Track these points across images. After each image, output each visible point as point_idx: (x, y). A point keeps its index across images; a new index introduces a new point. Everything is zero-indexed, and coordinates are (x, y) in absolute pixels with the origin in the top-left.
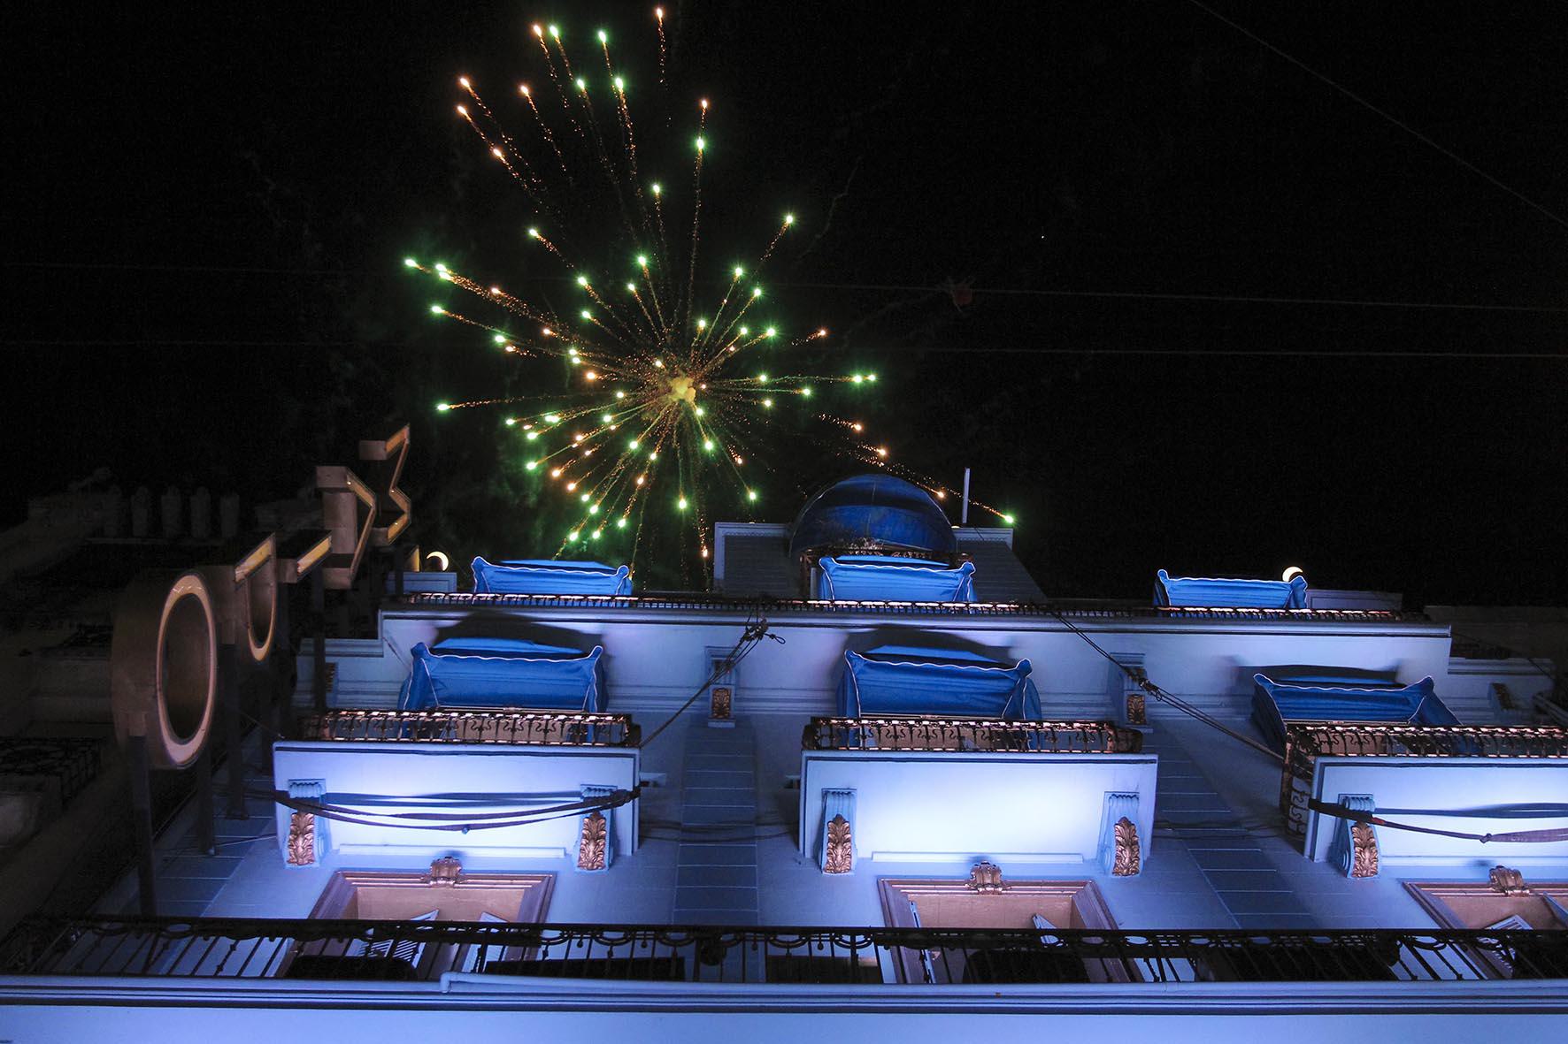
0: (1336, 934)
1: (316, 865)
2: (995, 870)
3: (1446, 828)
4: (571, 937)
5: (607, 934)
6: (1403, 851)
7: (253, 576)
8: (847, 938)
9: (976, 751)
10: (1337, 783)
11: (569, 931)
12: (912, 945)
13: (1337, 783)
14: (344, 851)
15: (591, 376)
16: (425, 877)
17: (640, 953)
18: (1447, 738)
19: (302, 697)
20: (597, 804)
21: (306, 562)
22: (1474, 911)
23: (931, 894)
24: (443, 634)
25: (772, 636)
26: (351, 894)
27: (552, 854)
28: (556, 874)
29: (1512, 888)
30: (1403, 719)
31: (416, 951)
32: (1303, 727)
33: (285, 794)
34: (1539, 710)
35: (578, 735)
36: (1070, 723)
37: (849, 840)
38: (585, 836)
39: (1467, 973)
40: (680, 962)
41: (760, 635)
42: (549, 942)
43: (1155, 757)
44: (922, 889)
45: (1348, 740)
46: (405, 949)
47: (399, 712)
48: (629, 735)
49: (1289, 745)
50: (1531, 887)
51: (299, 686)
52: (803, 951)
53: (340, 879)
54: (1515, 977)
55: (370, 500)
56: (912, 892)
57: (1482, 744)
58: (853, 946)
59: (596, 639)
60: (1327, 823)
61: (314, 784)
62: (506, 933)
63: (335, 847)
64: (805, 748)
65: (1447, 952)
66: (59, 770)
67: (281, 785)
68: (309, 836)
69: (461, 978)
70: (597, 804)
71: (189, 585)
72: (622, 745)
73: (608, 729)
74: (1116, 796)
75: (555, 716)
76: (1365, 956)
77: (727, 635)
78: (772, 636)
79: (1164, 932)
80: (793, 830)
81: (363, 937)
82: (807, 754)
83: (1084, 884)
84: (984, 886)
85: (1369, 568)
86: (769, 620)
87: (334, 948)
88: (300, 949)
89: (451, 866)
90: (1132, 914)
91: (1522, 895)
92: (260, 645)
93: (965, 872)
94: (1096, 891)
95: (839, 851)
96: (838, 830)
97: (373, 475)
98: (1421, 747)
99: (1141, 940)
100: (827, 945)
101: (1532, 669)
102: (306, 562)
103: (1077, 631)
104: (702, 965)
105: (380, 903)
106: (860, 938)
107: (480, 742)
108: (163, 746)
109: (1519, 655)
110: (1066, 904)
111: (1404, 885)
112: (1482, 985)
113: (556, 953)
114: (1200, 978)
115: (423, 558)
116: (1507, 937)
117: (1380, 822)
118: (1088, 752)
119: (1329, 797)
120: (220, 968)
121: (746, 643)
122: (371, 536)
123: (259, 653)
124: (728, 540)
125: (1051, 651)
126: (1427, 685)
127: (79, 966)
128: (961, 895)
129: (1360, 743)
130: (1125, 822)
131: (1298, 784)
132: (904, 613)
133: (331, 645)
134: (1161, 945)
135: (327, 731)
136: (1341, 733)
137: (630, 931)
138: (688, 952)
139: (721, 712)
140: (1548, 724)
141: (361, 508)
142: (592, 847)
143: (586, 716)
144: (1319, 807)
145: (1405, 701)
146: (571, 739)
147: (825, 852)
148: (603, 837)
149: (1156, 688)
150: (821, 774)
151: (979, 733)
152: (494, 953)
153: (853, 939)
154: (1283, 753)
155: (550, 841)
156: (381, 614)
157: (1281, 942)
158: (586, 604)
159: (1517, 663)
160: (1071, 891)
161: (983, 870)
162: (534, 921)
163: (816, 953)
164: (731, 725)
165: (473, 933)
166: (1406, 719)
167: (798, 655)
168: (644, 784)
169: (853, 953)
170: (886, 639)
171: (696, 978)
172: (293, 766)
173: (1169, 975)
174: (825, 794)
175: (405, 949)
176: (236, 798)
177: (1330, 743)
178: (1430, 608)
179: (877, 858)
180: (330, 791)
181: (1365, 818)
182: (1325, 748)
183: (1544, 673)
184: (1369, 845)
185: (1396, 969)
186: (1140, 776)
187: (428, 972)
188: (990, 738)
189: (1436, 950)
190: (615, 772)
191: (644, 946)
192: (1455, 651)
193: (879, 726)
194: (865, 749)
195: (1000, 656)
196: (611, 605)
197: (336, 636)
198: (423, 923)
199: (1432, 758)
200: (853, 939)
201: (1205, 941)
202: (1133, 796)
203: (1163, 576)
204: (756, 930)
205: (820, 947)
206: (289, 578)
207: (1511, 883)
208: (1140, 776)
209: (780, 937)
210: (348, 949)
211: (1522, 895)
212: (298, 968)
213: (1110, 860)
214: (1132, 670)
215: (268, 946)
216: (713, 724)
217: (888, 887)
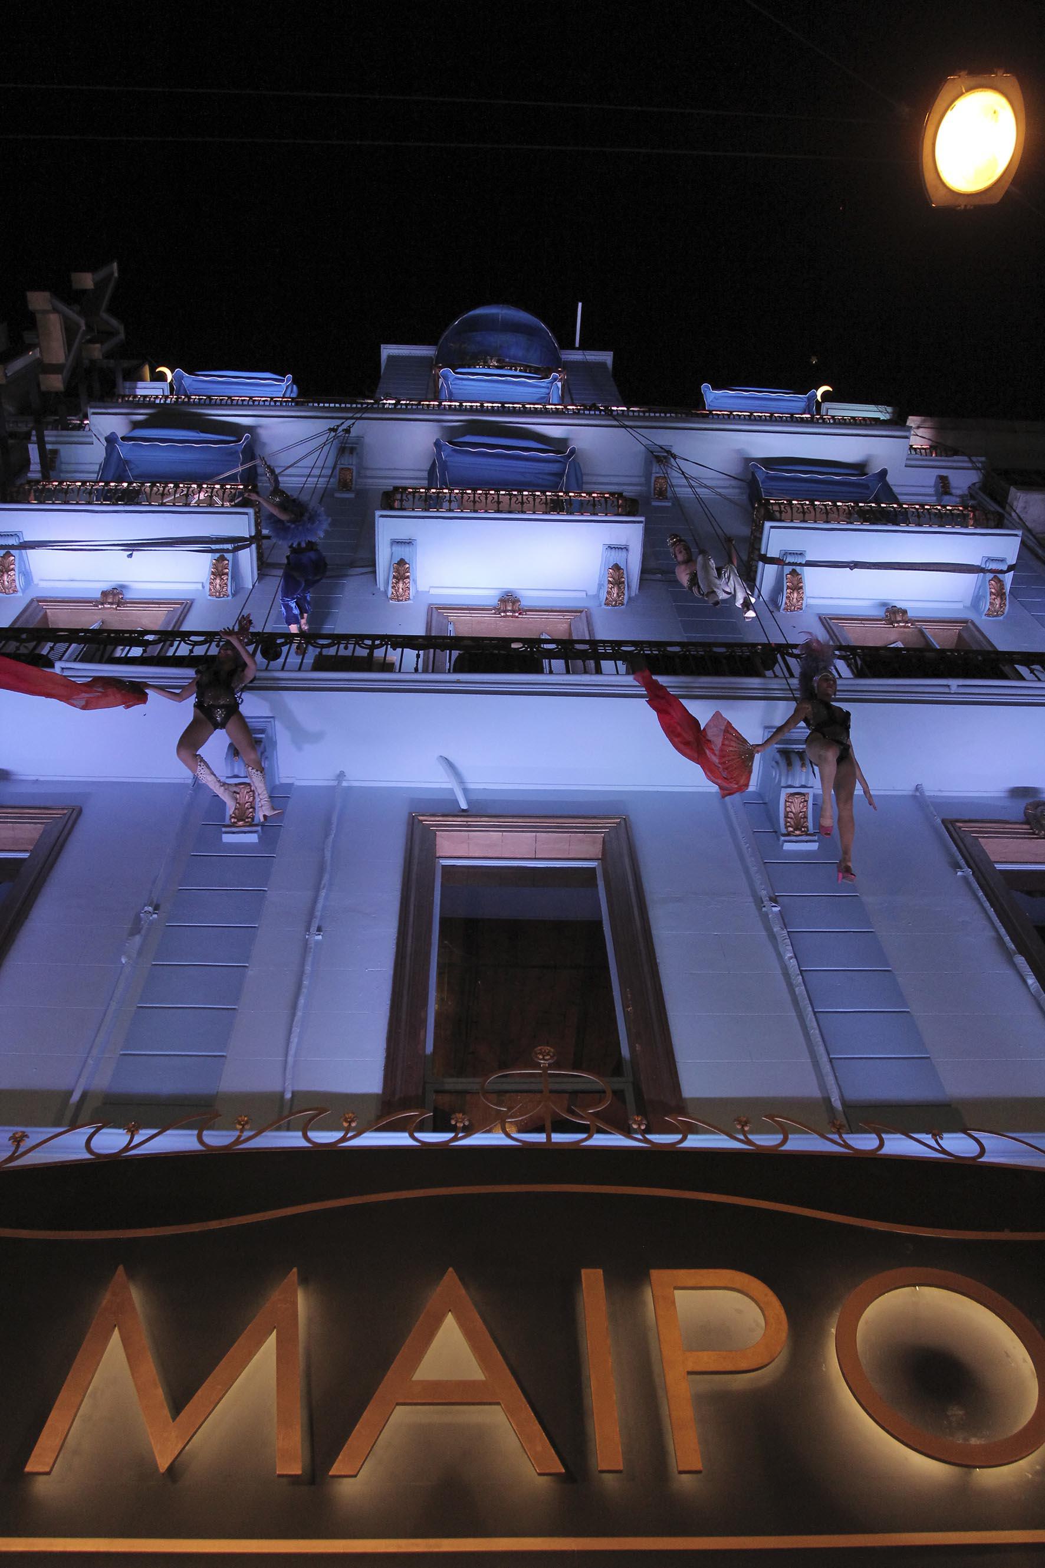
1: (20, 594)
5: (193, 638)
8: (369, 642)
9: (510, 512)
14: (43, 584)
16: (96, 603)
23: (466, 617)
24: (136, 425)
26: (41, 614)
29: (898, 622)
37: (408, 577)
38: (213, 573)
44: (459, 613)
50: (913, 622)
51: (32, 467)
53: (35, 604)
56: (453, 616)
57: (896, 515)
59: (250, 429)
63: (36, 581)
68: (11, 573)
70: (220, 548)
83: (581, 612)
84: (505, 612)
89: (114, 595)
91: (904, 627)
93: (495, 602)
95: (401, 585)
96: (401, 571)
100: (351, 647)
101: (970, 465)
103: (625, 427)
106: (377, 642)
109: (963, 454)
110: (565, 626)
111: (820, 618)
119: (772, 553)
124: (391, 358)
125: (601, 443)
126: (884, 473)
128: (488, 617)
130: (616, 567)
132: (492, 412)
134: (616, 650)
139: (345, 485)
142: (218, 581)
145: (866, 486)
147: (391, 585)
148: (227, 574)
153: (373, 642)
157: (689, 651)
158: (252, 403)
159: (961, 460)
160: (569, 616)
161: (509, 602)
164: (352, 495)
167: (406, 443)
170: (479, 429)
174: (396, 542)
179: (433, 591)
183: (977, 469)
185: (769, 673)
186: (629, 534)
190: (240, 525)
195: (559, 445)
196: (273, 403)
200: (373, 642)
202: (625, 548)
203: (706, 389)
205: (346, 648)
207: (899, 619)
208: (629, 534)
211: (904, 627)
213: (603, 595)
214: (662, 457)
216: (337, 495)
217: (435, 610)
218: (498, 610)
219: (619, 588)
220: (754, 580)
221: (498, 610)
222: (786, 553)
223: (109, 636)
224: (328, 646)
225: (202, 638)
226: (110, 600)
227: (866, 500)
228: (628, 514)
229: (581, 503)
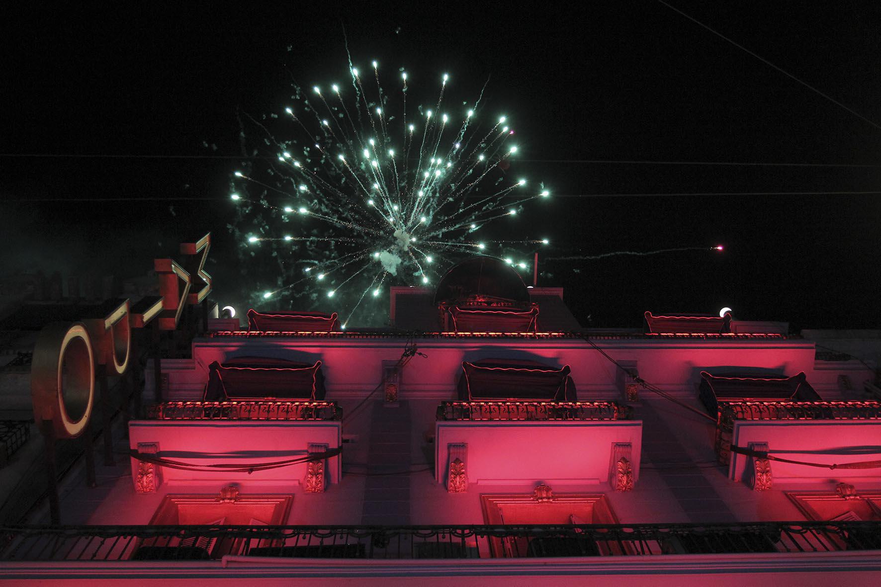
0: (743, 525)
2: (548, 489)
3: (808, 460)
4: (299, 534)
5: (320, 531)
6: (783, 473)
7: (118, 324)
8: (459, 531)
9: (537, 420)
10: (746, 436)
11: (299, 529)
12: (500, 535)
13: (746, 436)
14: (170, 483)
15: (288, 210)
17: (339, 542)
18: (810, 408)
19: (148, 392)
20: (317, 456)
21: (148, 315)
22: (829, 508)
25: (420, 354)
27: (291, 483)
28: (293, 495)
29: (849, 496)
30: (786, 396)
31: (209, 543)
32: (728, 403)
33: (136, 451)
34: (867, 390)
35: (307, 414)
36: (592, 403)
39: (829, 546)
40: (362, 546)
41: (413, 353)
42: (287, 536)
43: (641, 422)
45: (753, 410)
46: (201, 542)
47: (202, 402)
48: (335, 414)
49: (719, 414)
52: (433, 539)
54: (848, 549)
55: (185, 277)
56: (500, 503)
58: (463, 536)
59: (319, 356)
60: (741, 459)
61: (154, 445)
62: (258, 532)
64: (438, 419)
65: (808, 535)
66: (6, 438)
67: (133, 446)
69: (234, 558)
70: (317, 456)
71: (77, 331)
72: (332, 419)
73: (324, 409)
74: (618, 445)
75: (293, 403)
76: (759, 538)
77: (393, 352)
78: (420, 354)
79: (644, 526)
80: (432, 468)
81: (178, 535)
82: (438, 423)
84: (542, 499)
85: (773, 306)
86: (418, 345)
87: (161, 542)
88: (141, 544)
90: (628, 514)
92: (121, 364)
94: (607, 500)
95: (458, 479)
96: (758, 454)
97: (191, 263)
98: (796, 413)
99: (630, 530)
102: (148, 315)
103: (598, 348)
104: (375, 548)
105: (192, 512)
107: (249, 419)
108: (63, 425)
112: (828, 554)
113: (290, 543)
114: (665, 552)
115: (220, 309)
116: (841, 525)
117: (771, 458)
118: (602, 419)
119: (742, 444)
120: (94, 555)
121: (405, 358)
122: (188, 298)
123: (121, 369)
126: (802, 376)
127: (94, 555)
129: (760, 412)
131: (725, 436)
133: (165, 363)
134: (643, 533)
135: (161, 414)
136: (749, 406)
137: (333, 529)
138: (367, 541)
140: (870, 399)
141: (182, 283)
142: (314, 479)
143: (311, 403)
144: (737, 450)
146: (303, 416)
147: (450, 480)
149: (643, 381)
150: (448, 434)
151: (539, 410)
152: (254, 543)
153: (463, 531)
154: (716, 418)
155: (292, 476)
156: (194, 344)
161: (540, 487)
162: (280, 524)
163: (441, 540)
165: (245, 532)
166: (789, 396)
168: (344, 441)
169: (463, 539)
171: (371, 557)
172: (141, 434)
173: (646, 549)
174: (450, 446)
175: (201, 542)
176: (106, 452)
177: (743, 412)
178: (805, 332)
180: (161, 450)
181: (763, 456)
182: (740, 415)
184: (765, 472)
185: (778, 545)
186: (631, 434)
187: (216, 555)
188: (545, 412)
189: (801, 534)
190: (327, 435)
191: (341, 538)
192: (818, 356)
193: (499, 406)
194: (473, 420)
197: (167, 357)
198: (213, 526)
199: (855, 420)
200: (463, 531)
201: (540, 530)
202: (628, 445)
204: (444, 527)
206: (139, 325)
207: (848, 493)
208: (631, 434)
209: (420, 531)
210: (169, 540)
211: (854, 499)
212: (140, 555)
215: (123, 542)
217: (486, 500)
218: (532, 495)
219: (628, 477)
220: (728, 466)
221: (532, 495)
222: (753, 445)
223: (251, 531)
224: (430, 535)
225: (328, 531)
226: (228, 496)
227: (796, 397)
228: (627, 419)
229: (591, 410)
